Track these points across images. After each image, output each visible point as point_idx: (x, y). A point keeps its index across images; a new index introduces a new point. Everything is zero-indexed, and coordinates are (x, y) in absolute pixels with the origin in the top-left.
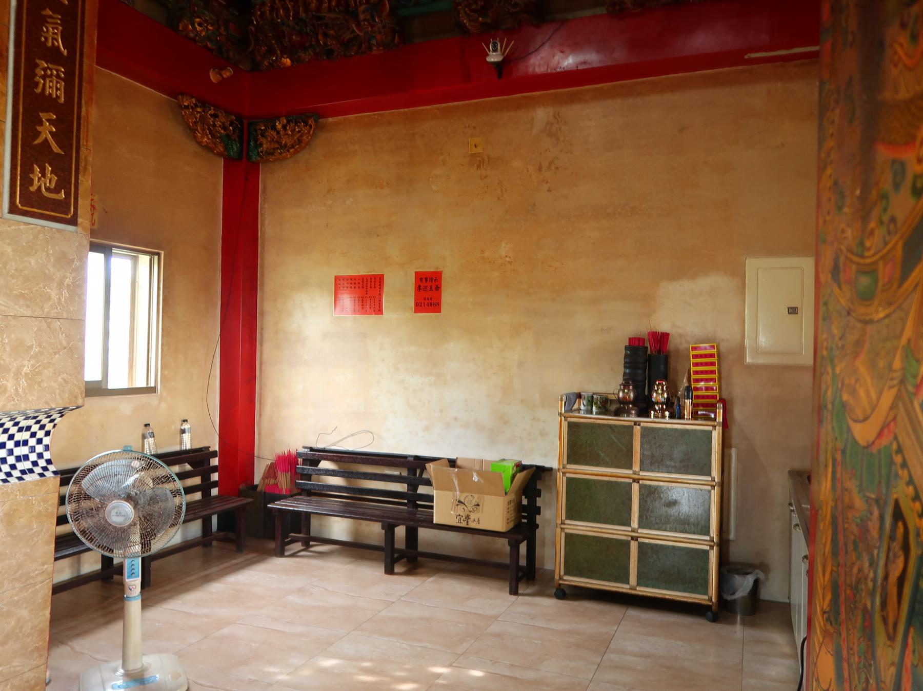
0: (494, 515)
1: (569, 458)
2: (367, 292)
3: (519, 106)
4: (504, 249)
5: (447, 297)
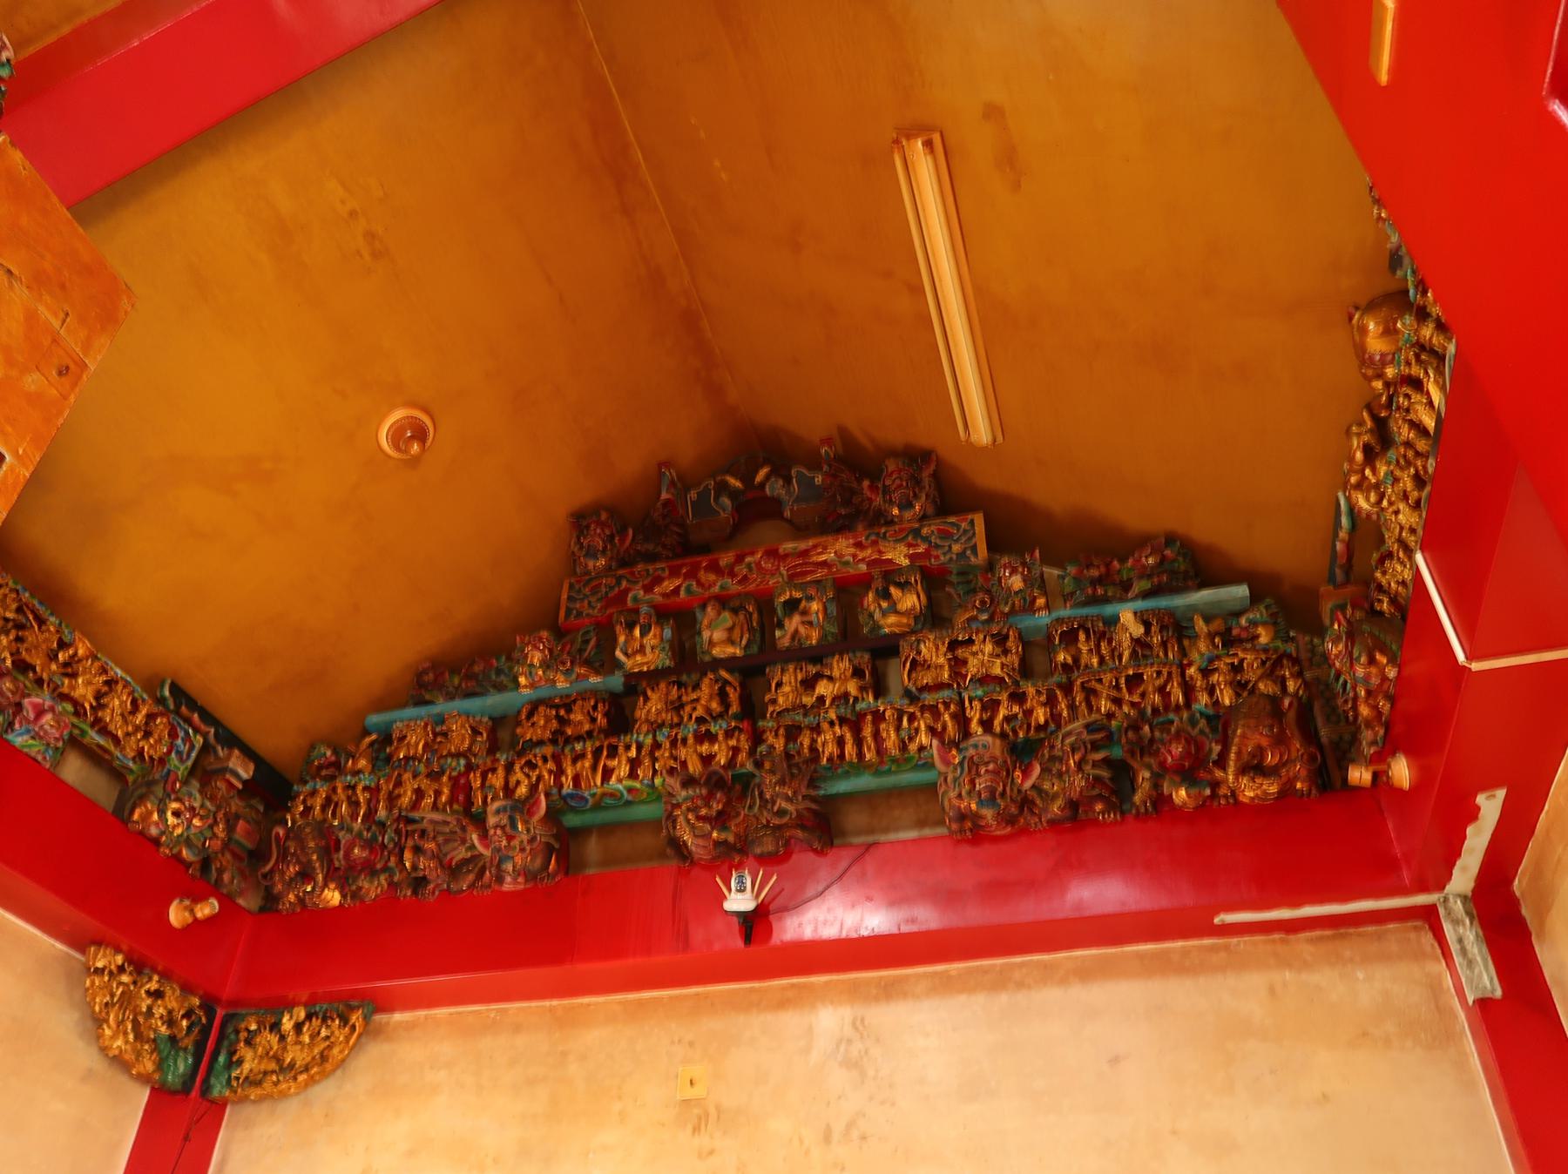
3: (782, 1004)
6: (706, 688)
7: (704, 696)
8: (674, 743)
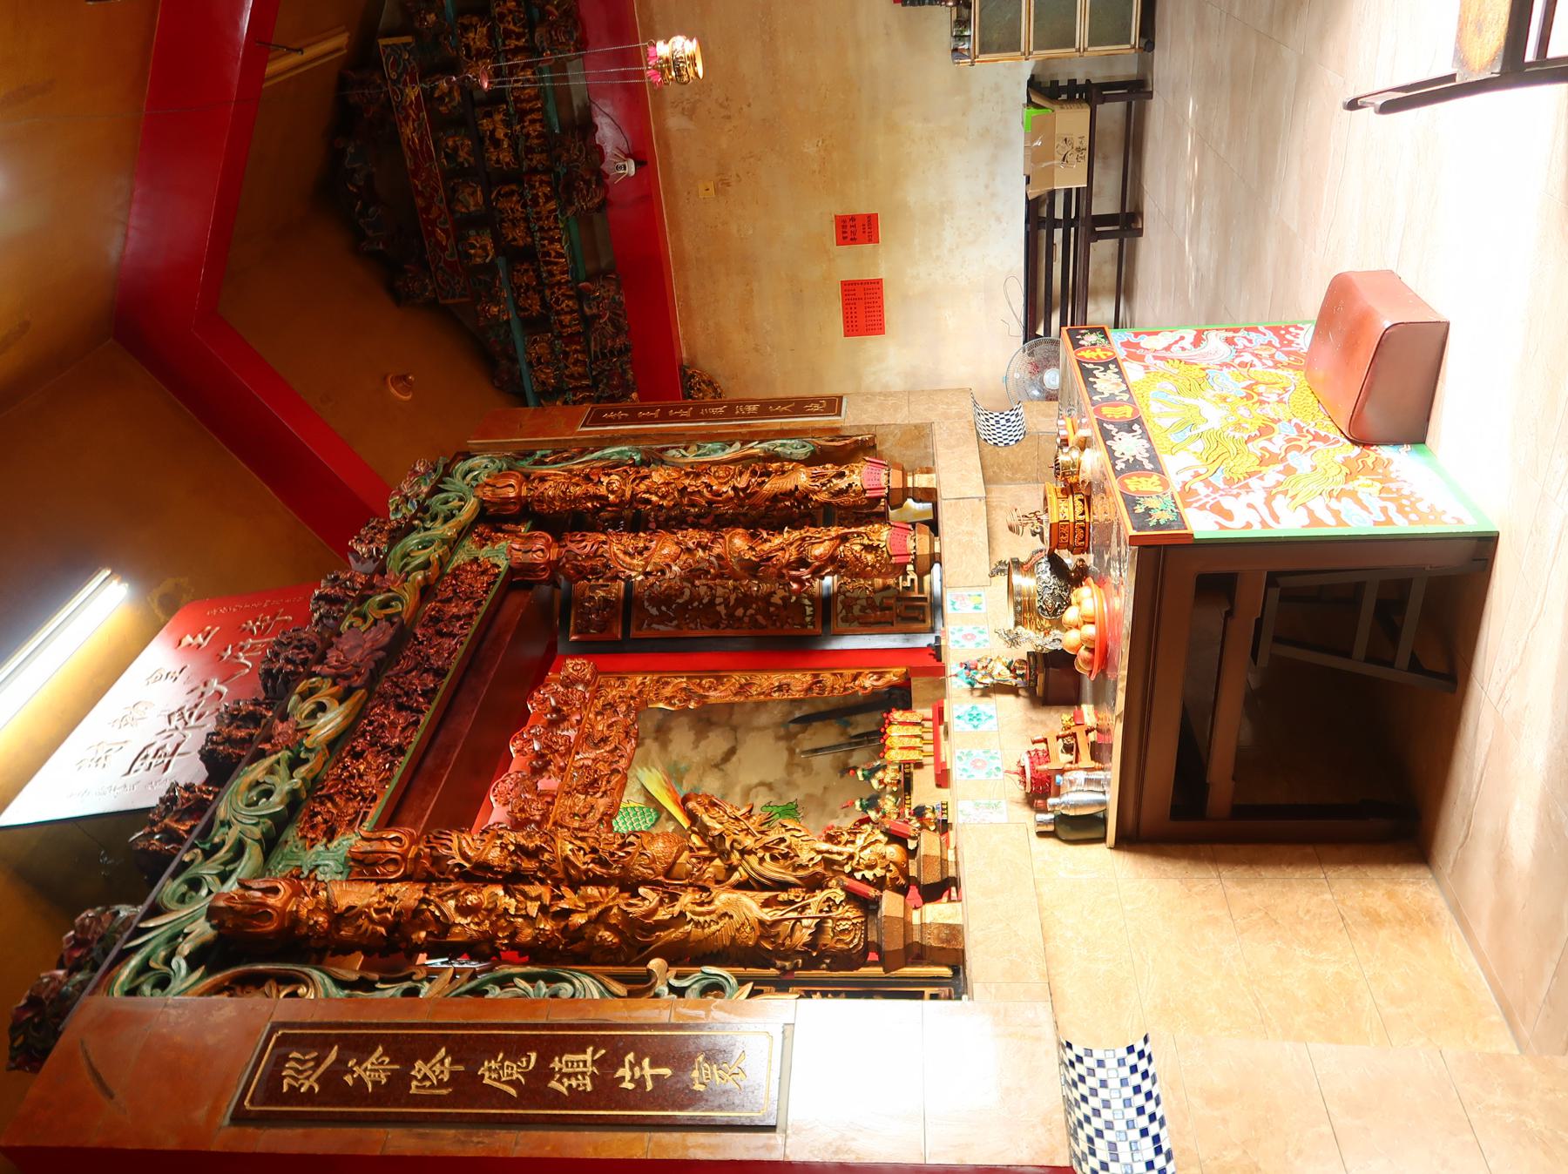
0: (1073, 121)
1: (1014, 50)
2: (863, 308)
3: (666, 147)
4: (810, 149)
5: (862, 209)
6: (504, 204)
7: (511, 206)
8: (539, 219)
